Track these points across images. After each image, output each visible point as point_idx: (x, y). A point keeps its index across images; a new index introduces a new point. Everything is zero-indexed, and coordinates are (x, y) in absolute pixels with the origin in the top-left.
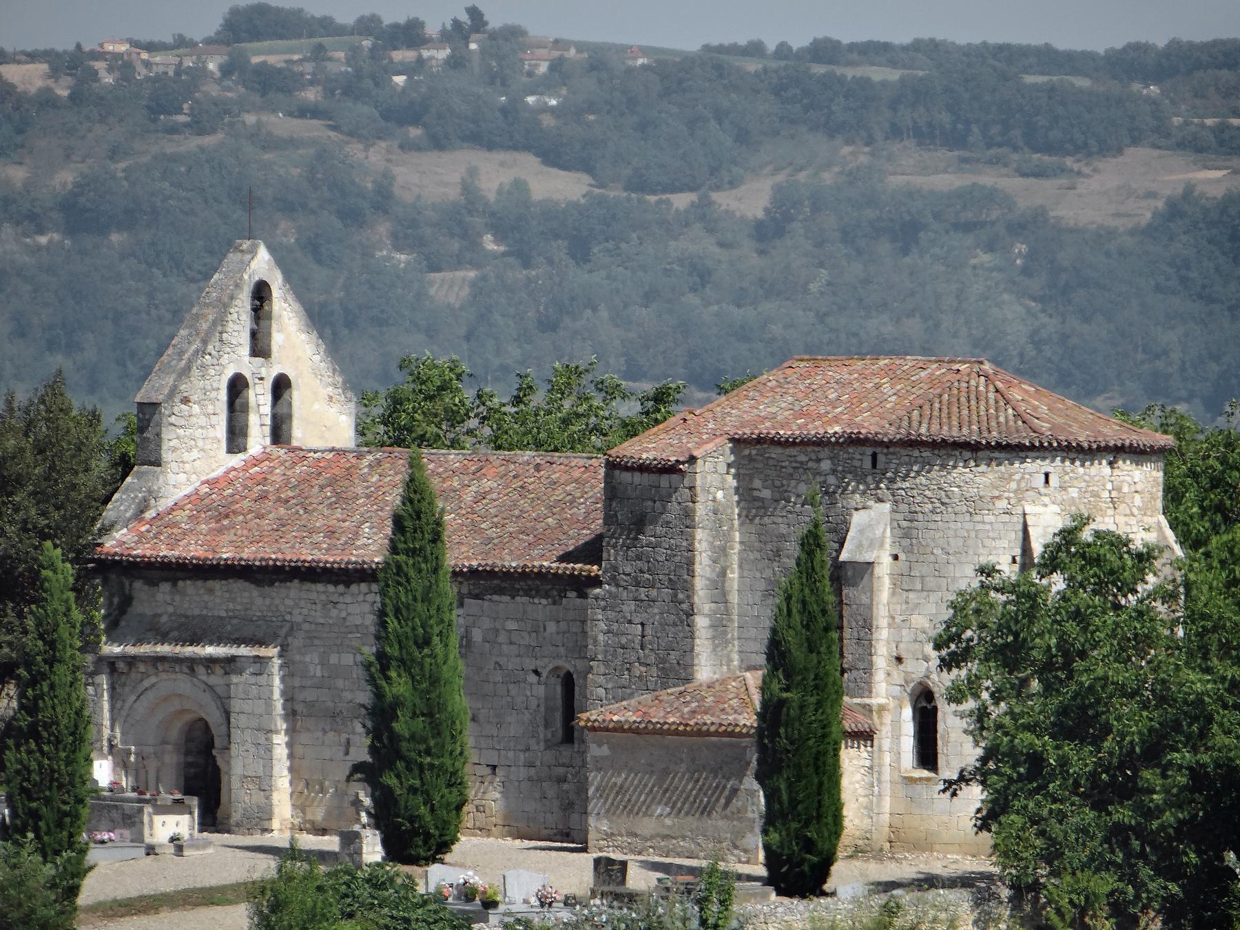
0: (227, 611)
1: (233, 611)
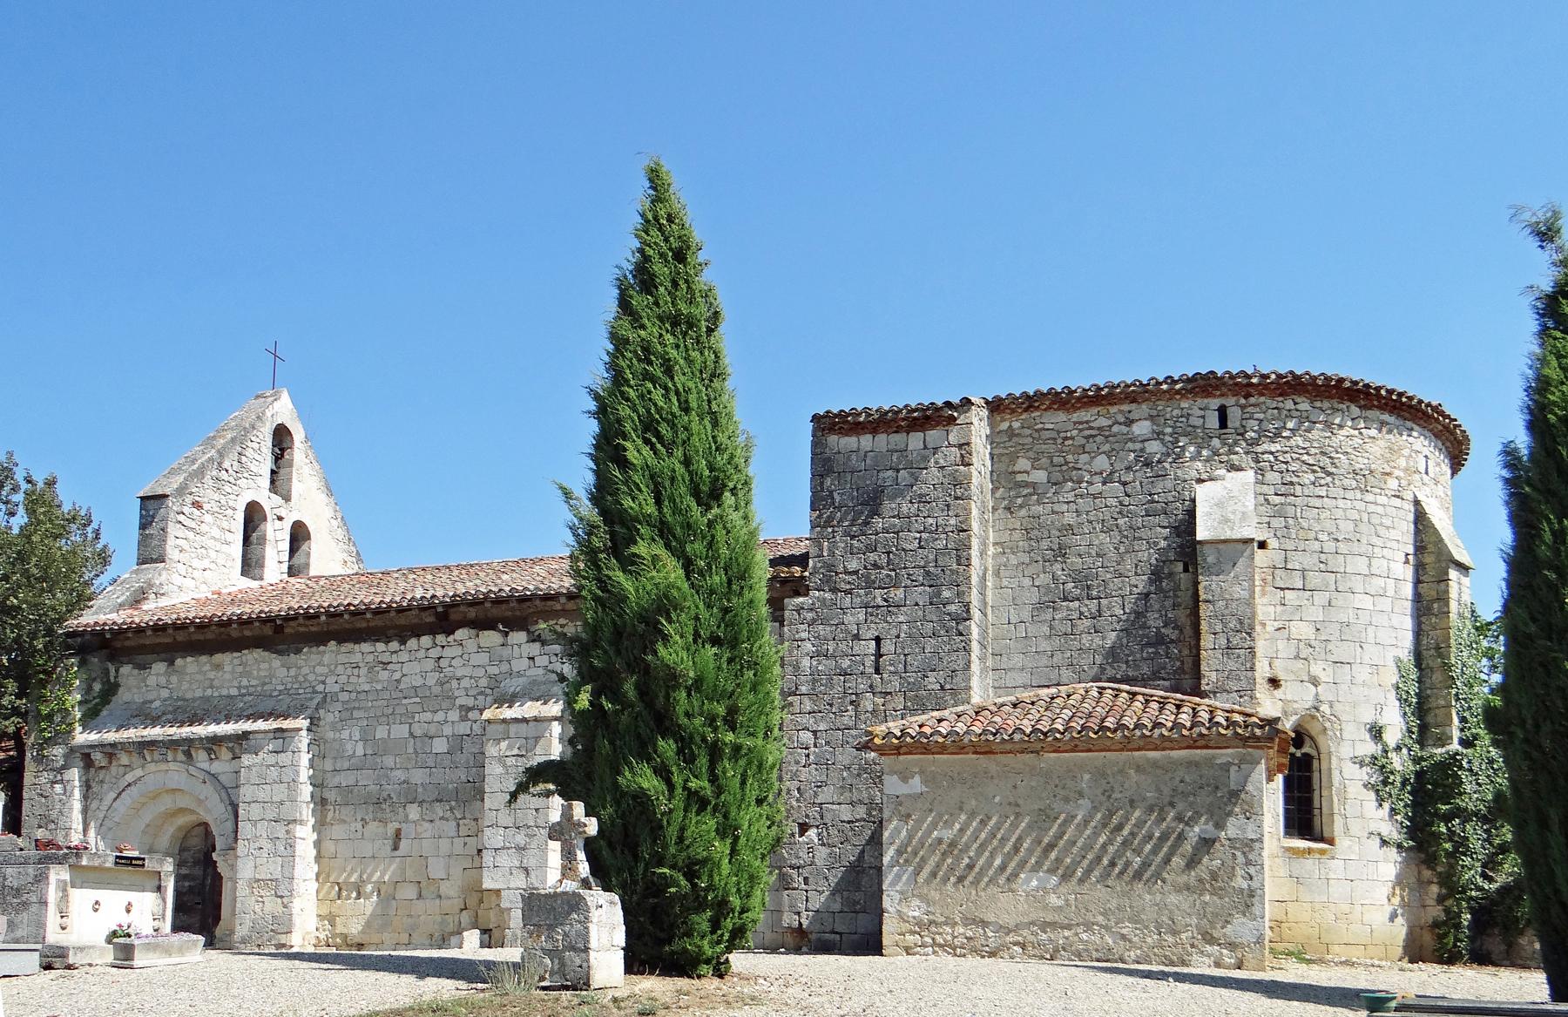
0: (239, 688)
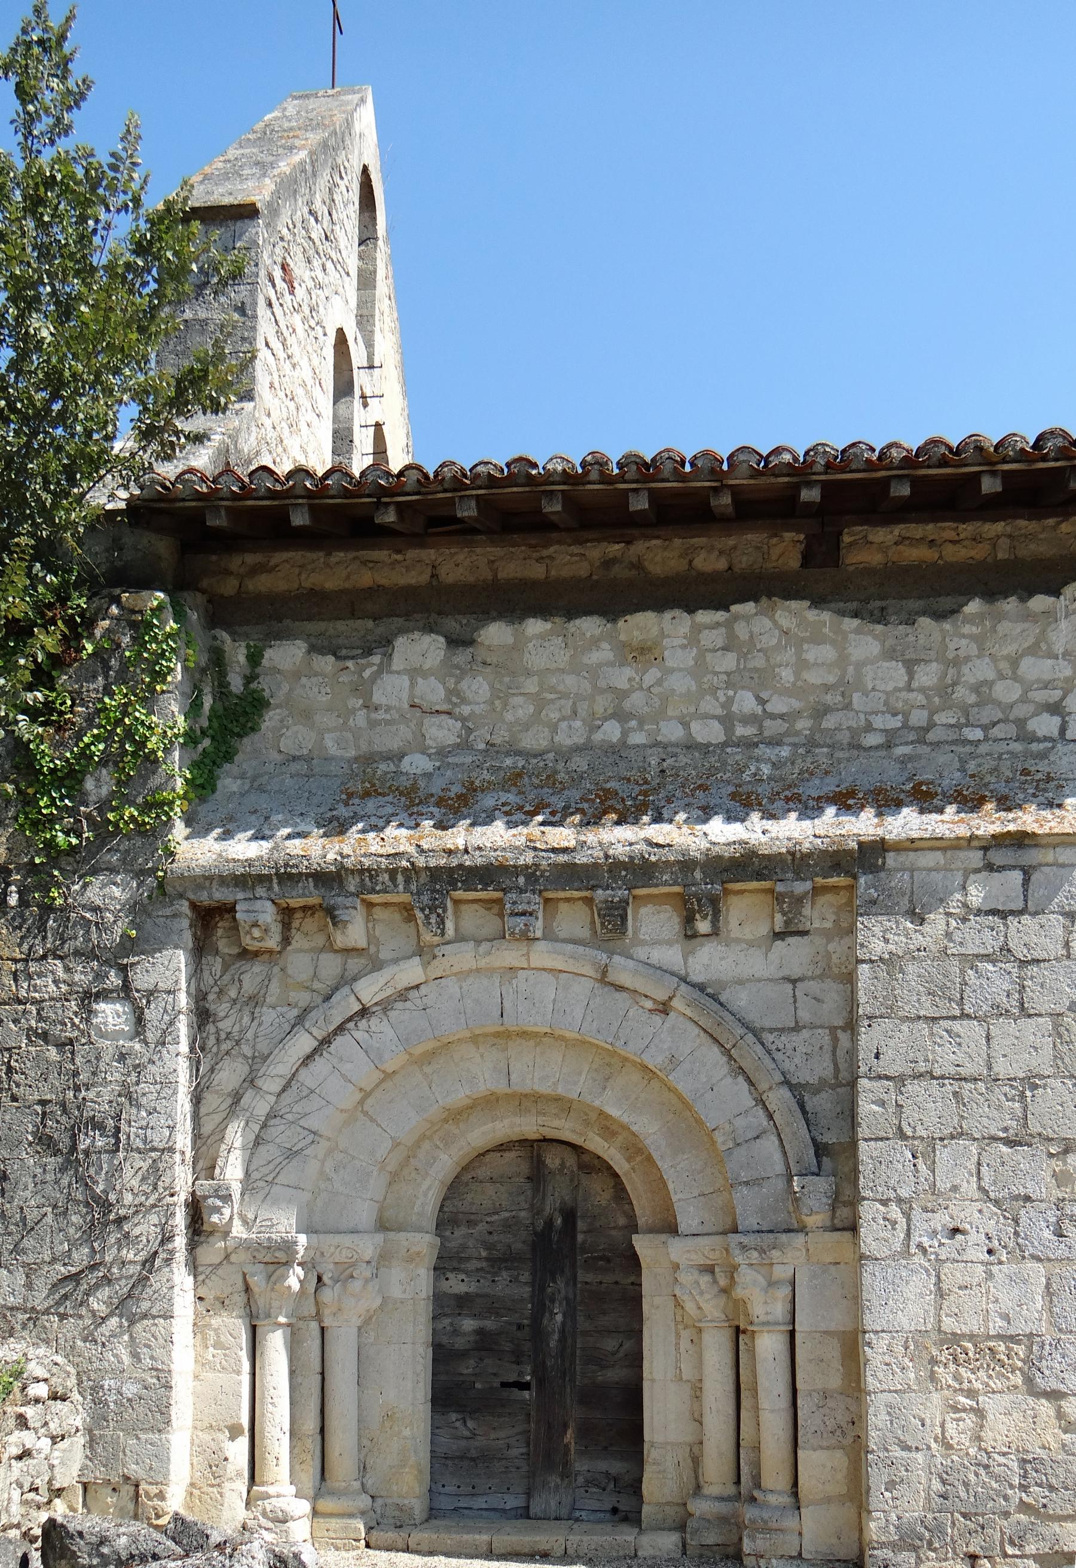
0: (727, 720)
1: (749, 719)
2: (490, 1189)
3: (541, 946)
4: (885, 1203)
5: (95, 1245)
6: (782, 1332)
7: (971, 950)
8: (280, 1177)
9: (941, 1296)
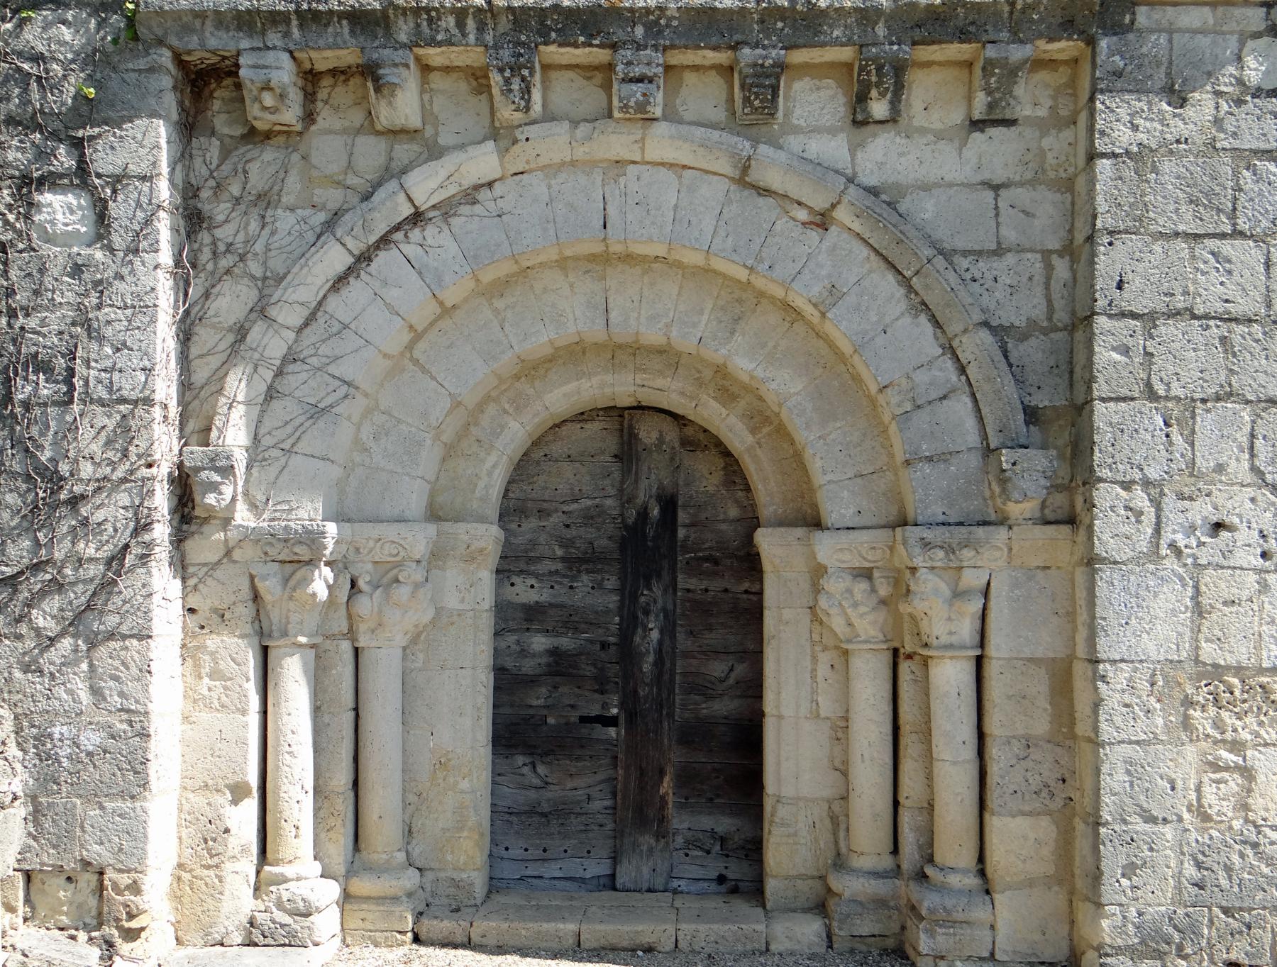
2: (568, 470)
3: (662, 128)
4: (1127, 486)
5: (40, 535)
6: (968, 658)
7: (1248, 143)
8: (300, 445)
9: (1200, 614)
